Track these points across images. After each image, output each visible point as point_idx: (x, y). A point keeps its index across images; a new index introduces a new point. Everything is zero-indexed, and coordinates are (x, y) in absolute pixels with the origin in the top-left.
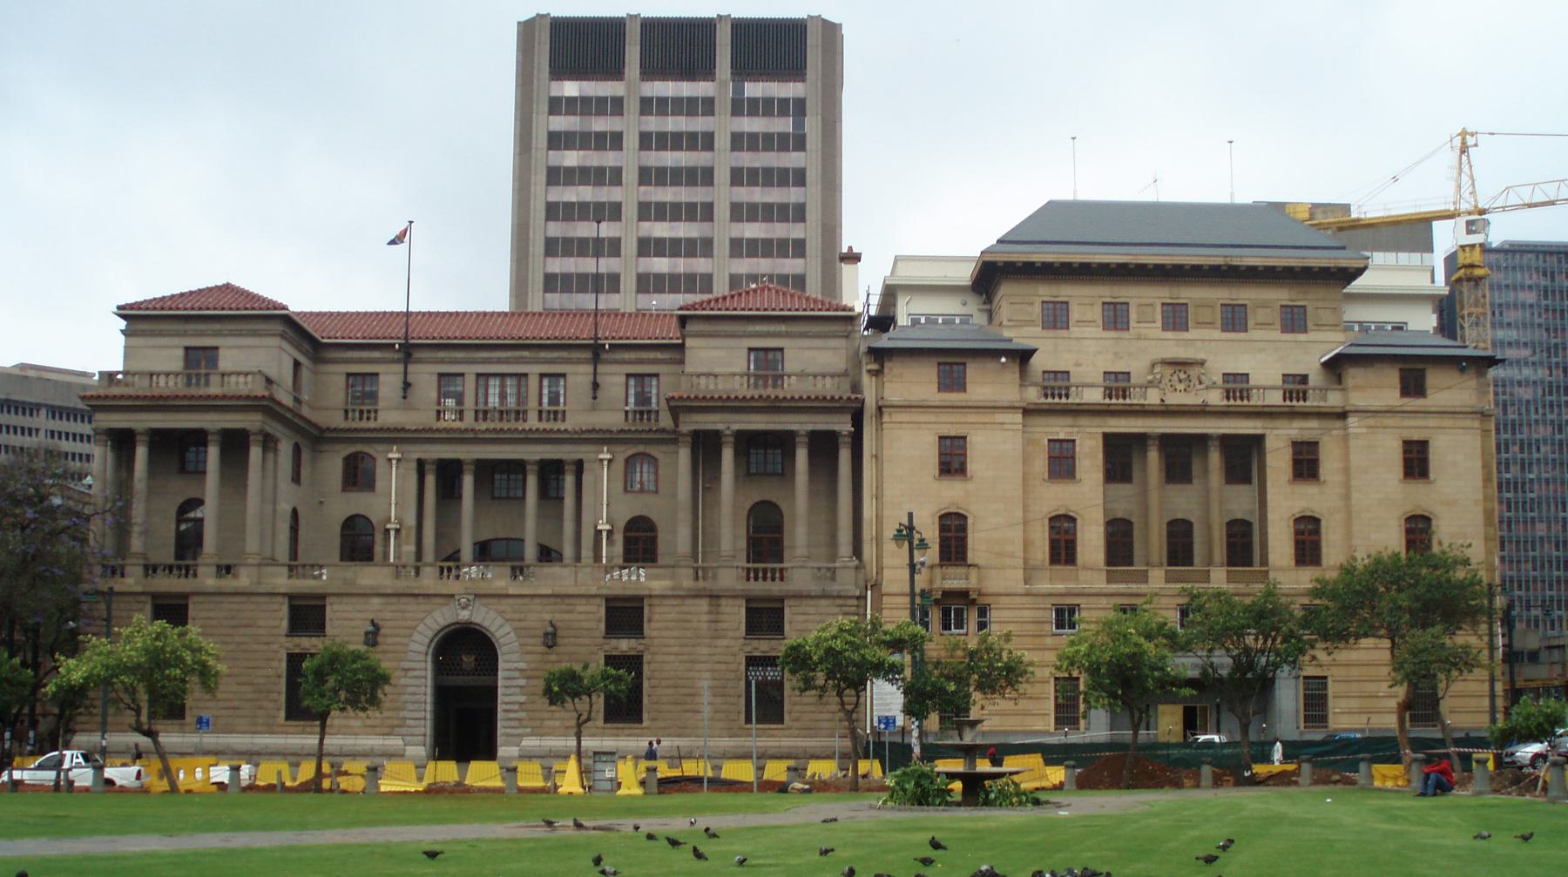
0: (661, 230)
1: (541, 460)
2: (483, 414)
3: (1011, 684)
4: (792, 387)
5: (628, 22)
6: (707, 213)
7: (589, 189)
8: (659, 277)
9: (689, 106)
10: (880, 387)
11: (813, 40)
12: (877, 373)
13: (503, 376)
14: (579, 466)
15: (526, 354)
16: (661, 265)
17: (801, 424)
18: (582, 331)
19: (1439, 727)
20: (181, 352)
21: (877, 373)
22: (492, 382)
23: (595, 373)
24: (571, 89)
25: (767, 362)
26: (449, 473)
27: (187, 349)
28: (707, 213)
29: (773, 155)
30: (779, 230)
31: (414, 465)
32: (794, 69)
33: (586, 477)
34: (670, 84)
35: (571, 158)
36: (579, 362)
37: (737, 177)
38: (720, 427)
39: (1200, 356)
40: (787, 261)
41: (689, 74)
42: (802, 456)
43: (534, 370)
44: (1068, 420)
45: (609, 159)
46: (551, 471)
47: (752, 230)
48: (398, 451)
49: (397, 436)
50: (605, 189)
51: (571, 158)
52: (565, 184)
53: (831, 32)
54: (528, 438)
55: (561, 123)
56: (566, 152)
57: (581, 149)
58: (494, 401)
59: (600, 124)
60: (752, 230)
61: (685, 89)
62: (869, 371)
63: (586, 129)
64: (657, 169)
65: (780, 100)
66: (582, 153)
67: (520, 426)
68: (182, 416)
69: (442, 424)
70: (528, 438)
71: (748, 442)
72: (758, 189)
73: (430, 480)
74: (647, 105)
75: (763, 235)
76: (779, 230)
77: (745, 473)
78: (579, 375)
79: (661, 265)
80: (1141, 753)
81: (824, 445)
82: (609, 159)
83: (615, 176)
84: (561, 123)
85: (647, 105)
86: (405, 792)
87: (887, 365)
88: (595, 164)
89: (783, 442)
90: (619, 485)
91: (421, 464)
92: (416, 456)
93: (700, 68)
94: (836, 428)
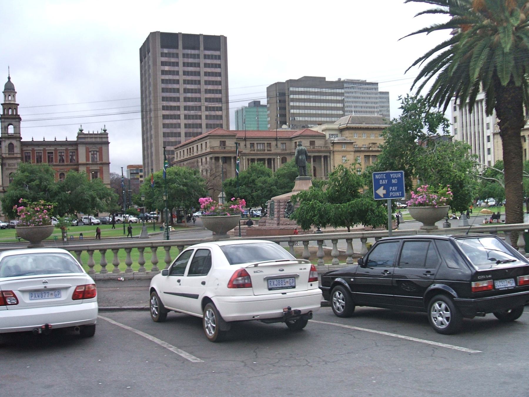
0: (189, 86)
2: (258, 150)
3: (354, 212)
5: (179, 35)
6: (199, 82)
7: (171, 76)
10: (333, 148)
11: (222, 41)
12: (333, 146)
13: (260, 143)
14: (274, 159)
16: (189, 95)
17: (323, 154)
21: (333, 146)
24: (166, 51)
25: (223, 143)
26: (217, 159)
28: (199, 82)
30: (216, 87)
33: (275, 161)
34: (189, 50)
35: (167, 68)
39: (376, 142)
41: (194, 48)
42: (323, 159)
43: (266, 142)
45: (176, 69)
46: (269, 160)
47: (210, 87)
50: (175, 76)
51: (167, 68)
54: (266, 154)
59: (173, 60)
60: (210, 87)
61: (193, 52)
63: (170, 61)
67: (264, 152)
70: (266, 154)
71: (315, 157)
72: (210, 77)
74: (206, 57)
75: (212, 88)
76: (216, 87)
78: (273, 143)
79: (189, 95)
81: (326, 157)
82: (176, 69)
84: (164, 59)
85: (206, 57)
86: (192, 245)
93: (196, 47)
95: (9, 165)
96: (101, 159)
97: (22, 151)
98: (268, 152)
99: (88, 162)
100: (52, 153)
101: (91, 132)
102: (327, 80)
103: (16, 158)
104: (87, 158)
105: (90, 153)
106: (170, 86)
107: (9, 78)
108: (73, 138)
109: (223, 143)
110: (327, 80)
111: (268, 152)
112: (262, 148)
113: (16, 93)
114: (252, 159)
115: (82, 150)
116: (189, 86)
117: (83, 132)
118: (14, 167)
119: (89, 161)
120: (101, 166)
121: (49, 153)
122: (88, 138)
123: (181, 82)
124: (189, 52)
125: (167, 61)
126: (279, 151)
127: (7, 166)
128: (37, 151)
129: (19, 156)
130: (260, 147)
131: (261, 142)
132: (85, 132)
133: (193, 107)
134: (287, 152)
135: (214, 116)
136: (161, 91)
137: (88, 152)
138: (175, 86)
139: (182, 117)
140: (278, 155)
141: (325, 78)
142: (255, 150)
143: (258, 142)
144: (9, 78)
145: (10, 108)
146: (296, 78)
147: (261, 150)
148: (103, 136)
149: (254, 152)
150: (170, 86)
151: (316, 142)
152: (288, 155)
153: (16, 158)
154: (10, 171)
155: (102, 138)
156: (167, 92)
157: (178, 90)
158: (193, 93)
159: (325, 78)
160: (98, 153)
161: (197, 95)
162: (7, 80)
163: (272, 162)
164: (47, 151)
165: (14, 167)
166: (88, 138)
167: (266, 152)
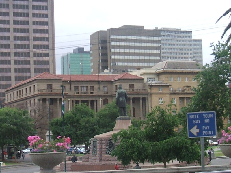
0: (18, 34)
2: (82, 93)
4: (54, 91)
7: (2, 25)
8: (18, 45)
9: (23, 7)
10: (151, 90)
12: (151, 89)
13: (84, 86)
14: (97, 101)
15: (85, 83)
16: (19, 42)
18: (97, 79)
19: (117, 159)
20: (46, 85)
21: (151, 89)
26: (44, 100)
27: (47, 84)
29: (41, 18)
31: (72, 101)
33: (98, 103)
36: (96, 84)
37: (15, 14)
38: (140, 97)
39: (190, 85)
40: (44, 42)
43: (89, 85)
44: (174, 95)
46: (92, 102)
47: (38, 35)
50: (6, 25)
54: (90, 96)
62: (149, 89)
67: (87, 94)
68: (54, 96)
69: (25, 88)
73: (74, 103)
77: (133, 102)
78: (96, 86)
79: (19, 42)
81: (144, 99)
88: (3, 19)
89: (138, 99)
92: (72, 100)
94: (145, 97)
98: (91, 94)
111: (91, 94)
112: (85, 90)
114: (76, 101)
116: (18, 34)
126: (101, 93)
130: (84, 90)
131: (84, 85)
139: (12, 62)
140: (100, 97)
147: (84, 93)
149: (78, 94)
151: (135, 85)
152: (109, 97)
158: (22, 40)
161: (26, 43)
163: (95, 103)
167: (89, 94)
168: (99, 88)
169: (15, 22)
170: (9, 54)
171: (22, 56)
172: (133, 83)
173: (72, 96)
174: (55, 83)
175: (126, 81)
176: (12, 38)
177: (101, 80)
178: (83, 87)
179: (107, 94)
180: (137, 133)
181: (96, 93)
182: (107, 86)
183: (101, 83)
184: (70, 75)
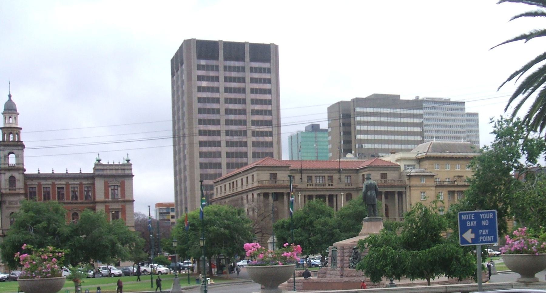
0: (231, 106)
1: (330, 195)
2: (316, 185)
5: (219, 43)
8: (231, 121)
10: (410, 181)
13: (319, 176)
14: (337, 195)
16: (232, 117)
17: (397, 190)
20: (269, 174)
22: (320, 177)
23: (340, 176)
24: (203, 62)
25: (384, 176)
26: (266, 195)
29: (262, 85)
32: (268, 60)
33: (338, 198)
35: (204, 84)
36: (336, 173)
39: (462, 175)
43: (326, 175)
45: (215, 84)
46: (331, 197)
47: (257, 107)
48: (300, 193)
49: (301, 190)
52: (203, 92)
53: (276, 47)
54: (327, 190)
55: (202, 73)
56: (202, 82)
57: (207, 81)
58: (318, 182)
64: (229, 88)
65: (263, 68)
66: (207, 82)
67: (324, 187)
71: (387, 193)
73: (307, 199)
78: (336, 176)
79: (232, 117)
80: (60, 254)
81: (400, 194)
82: (215, 84)
83: (217, 90)
84: (202, 73)
85: (252, 70)
87: (411, 179)
89: (393, 193)
90: (345, 199)
91: (305, 196)
92: (304, 194)
93: (241, 58)
95: (10, 203)
96: (123, 195)
97: (26, 185)
98: (330, 187)
99: (107, 200)
100: (63, 188)
101: (117, 163)
102: (402, 98)
103: (18, 195)
104: (106, 195)
105: (110, 189)
106: (208, 106)
107: (10, 96)
108: (89, 170)
109: (384, 176)
110: (402, 98)
112: (321, 182)
113: (18, 114)
115: (99, 185)
116: (231, 106)
117: (101, 162)
118: (14, 206)
119: (108, 198)
120: (123, 204)
121: (58, 188)
122: (107, 169)
123: (222, 100)
124: (232, 63)
125: (204, 75)
126: (342, 186)
127: (7, 205)
128: (73, 186)
129: (22, 191)
130: (320, 181)
132: (104, 162)
133: (236, 132)
134: (353, 187)
135: (262, 143)
136: (197, 111)
137: (107, 186)
138: (215, 106)
139: (223, 144)
141: (399, 96)
142: (314, 185)
143: (317, 175)
144: (10, 96)
145: (11, 133)
146: (364, 96)
147: (320, 185)
148: (126, 167)
149: (311, 187)
150: (208, 106)
151: (388, 174)
152: (354, 190)
153: (18, 195)
154: (11, 211)
155: (124, 169)
156: (205, 113)
157: (218, 111)
159: (399, 96)
160: (119, 189)
161: (242, 117)
162: (8, 98)
163: (335, 199)
164: (57, 186)
165: (14, 206)
166: (107, 169)
167: (327, 187)
168: (340, 178)
169: (227, 90)
170: (218, 133)
171: (236, 135)
172: (386, 172)
173: (303, 189)
174: (390, 172)
175: (376, 169)
176: (222, 112)
177: (342, 167)
178: (318, 177)
179: (350, 187)
180: (391, 239)
181: (336, 185)
182: (351, 176)
183: (343, 172)
184: (301, 161)
